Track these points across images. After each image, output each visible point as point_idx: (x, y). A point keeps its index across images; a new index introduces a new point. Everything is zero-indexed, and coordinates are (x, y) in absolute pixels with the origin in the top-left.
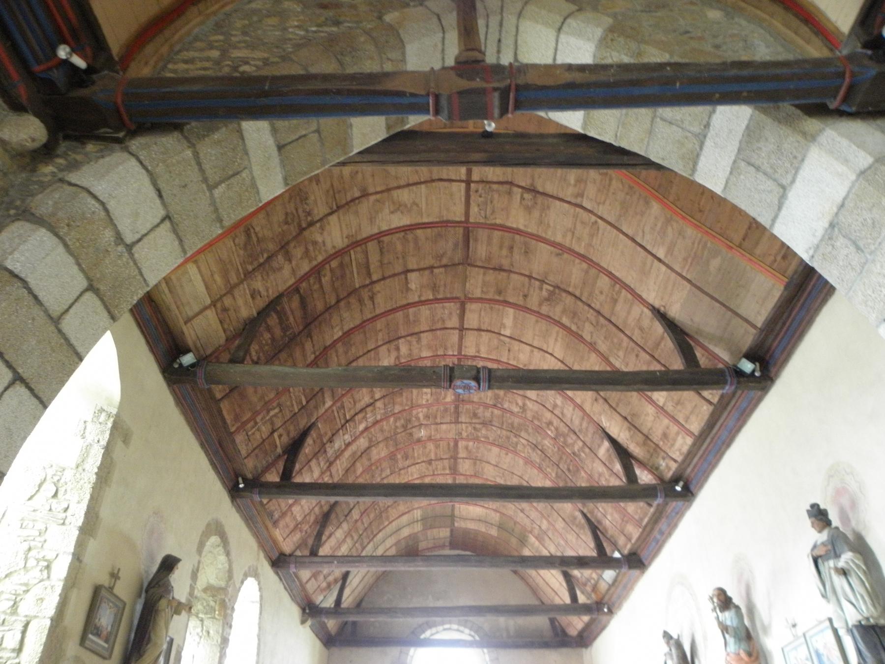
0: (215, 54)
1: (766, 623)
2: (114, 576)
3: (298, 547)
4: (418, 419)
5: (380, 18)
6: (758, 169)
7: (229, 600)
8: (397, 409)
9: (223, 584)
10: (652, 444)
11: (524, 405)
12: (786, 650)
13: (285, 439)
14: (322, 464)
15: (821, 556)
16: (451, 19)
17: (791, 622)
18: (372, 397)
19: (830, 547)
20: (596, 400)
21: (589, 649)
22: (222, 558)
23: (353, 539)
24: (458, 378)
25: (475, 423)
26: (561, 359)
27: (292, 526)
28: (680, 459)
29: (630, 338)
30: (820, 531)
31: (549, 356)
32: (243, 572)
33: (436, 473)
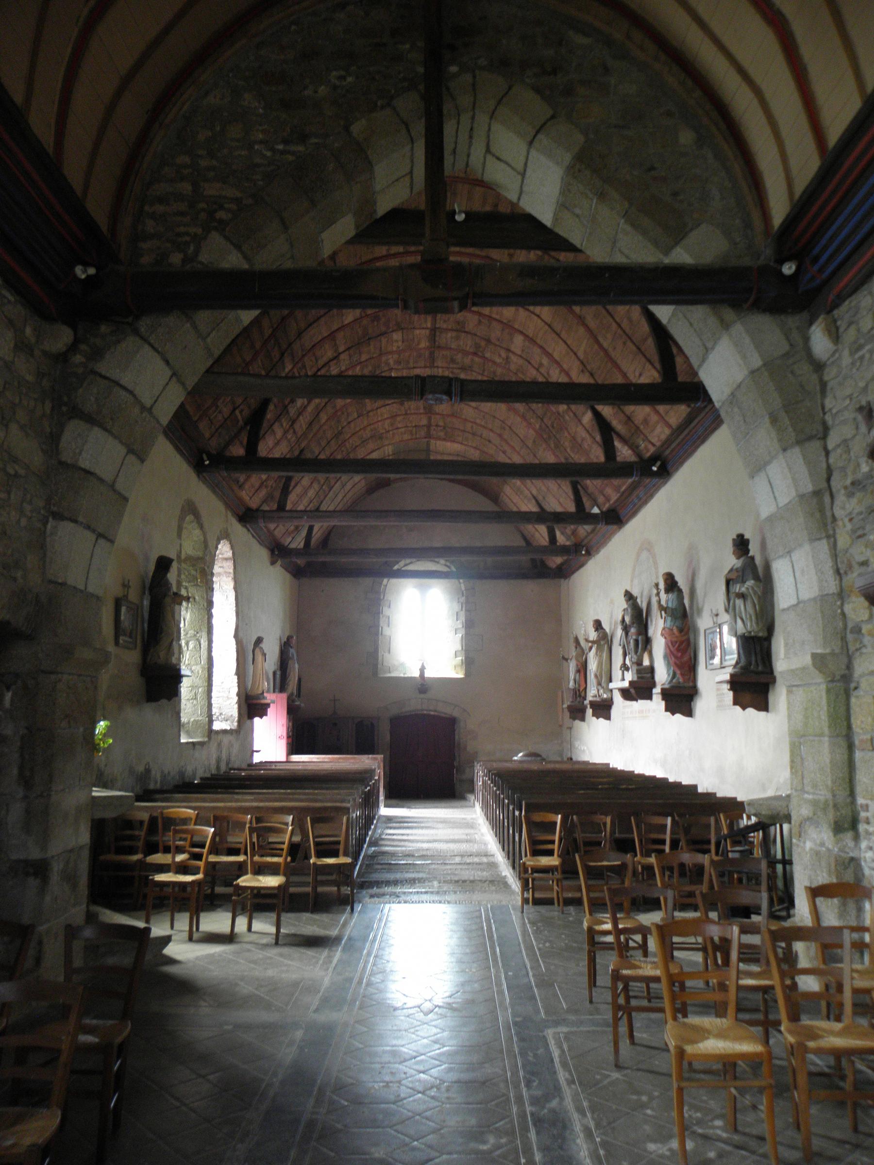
0: (186, 188)
1: (700, 606)
2: (126, 586)
3: (265, 501)
4: (387, 364)
5: (347, 129)
6: (691, 324)
7: (208, 567)
8: (364, 357)
9: (200, 554)
10: (633, 425)
11: (508, 358)
12: (708, 632)
13: (246, 412)
14: (284, 425)
15: (732, 579)
16: (419, 128)
17: (714, 612)
18: (335, 351)
19: (740, 574)
20: (582, 371)
21: (567, 580)
22: (197, 532)
23: (319, 483)
24: (430, 393)
25: (453, 368)
26: (549, 323)
27: (257, 485)
28: (658, 444)
29: (619, 325)
30: (738, 558)
31: (536, 318)
32: (216, 539)
33: (409, 412)
